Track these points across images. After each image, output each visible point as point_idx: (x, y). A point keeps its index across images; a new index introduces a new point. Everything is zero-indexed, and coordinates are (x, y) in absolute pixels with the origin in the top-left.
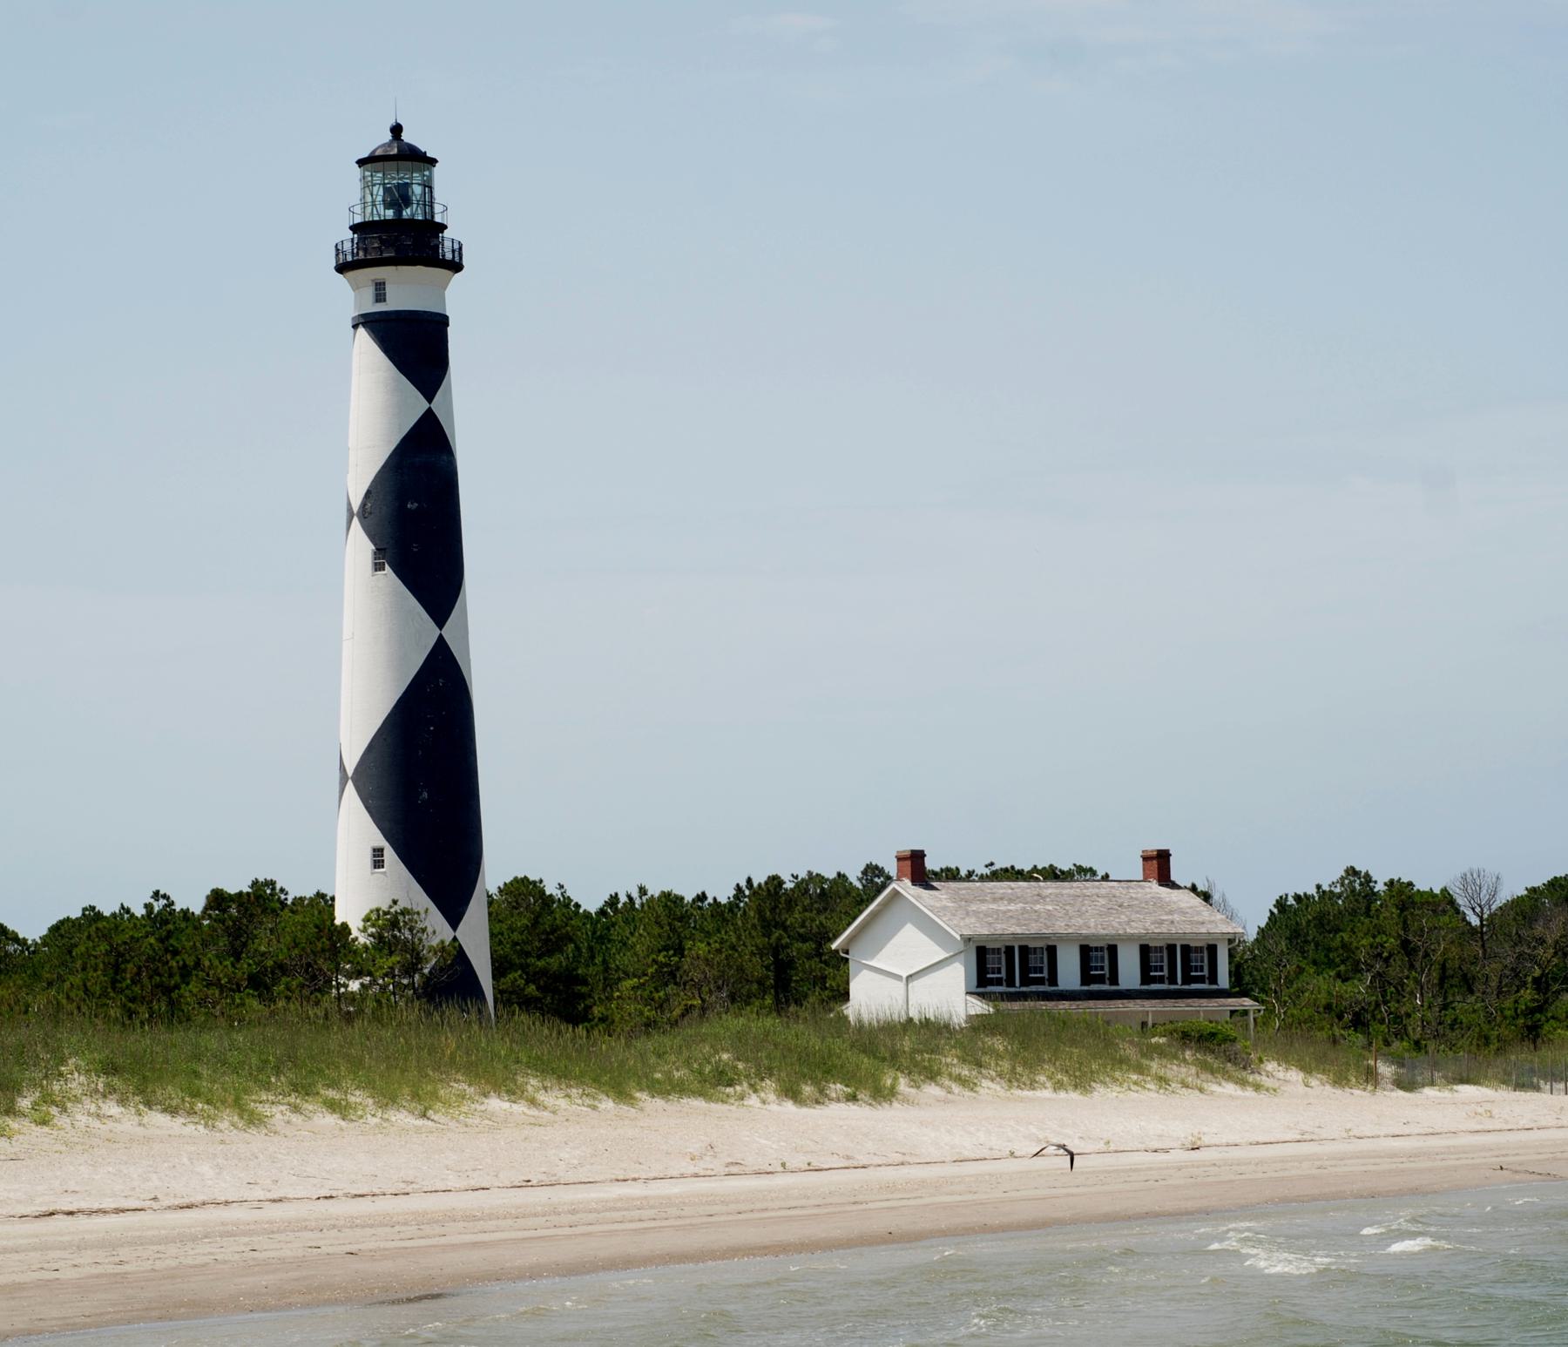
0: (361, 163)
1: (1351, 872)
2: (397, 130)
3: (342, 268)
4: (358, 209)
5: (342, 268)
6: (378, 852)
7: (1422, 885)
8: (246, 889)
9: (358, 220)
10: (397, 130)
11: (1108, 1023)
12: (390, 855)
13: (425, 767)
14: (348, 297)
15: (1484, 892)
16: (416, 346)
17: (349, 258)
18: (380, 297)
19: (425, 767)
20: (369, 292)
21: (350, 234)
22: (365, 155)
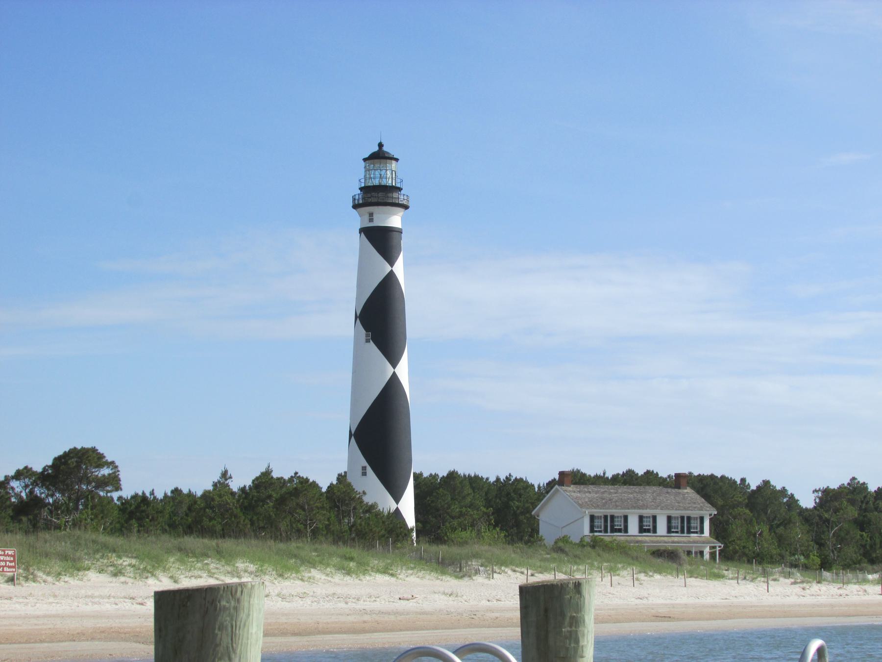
0: (365, 160)
1: (854, 479)
2: (381, 145)
3: (356, 206)
4: (363, 181)
5: (356, 206)
6: (364, 468)
7: (834, 486)
8: (211, 488)
9: (363, 185)
10: (381, 145)
11: (267, 596)
12: (369, 470)
13: (380, 431)
14: (356, 220)
15: (136, 530)
16: (382, 241)
17: (361, 202)
18: (371, 220)
19: (380, 431)
20: (367, 217)
21: (359, 192)
22: (367, 156)
